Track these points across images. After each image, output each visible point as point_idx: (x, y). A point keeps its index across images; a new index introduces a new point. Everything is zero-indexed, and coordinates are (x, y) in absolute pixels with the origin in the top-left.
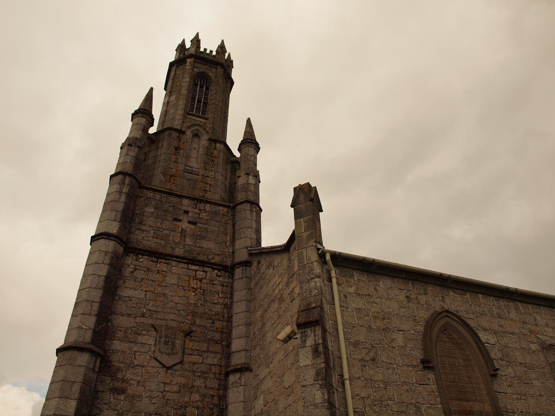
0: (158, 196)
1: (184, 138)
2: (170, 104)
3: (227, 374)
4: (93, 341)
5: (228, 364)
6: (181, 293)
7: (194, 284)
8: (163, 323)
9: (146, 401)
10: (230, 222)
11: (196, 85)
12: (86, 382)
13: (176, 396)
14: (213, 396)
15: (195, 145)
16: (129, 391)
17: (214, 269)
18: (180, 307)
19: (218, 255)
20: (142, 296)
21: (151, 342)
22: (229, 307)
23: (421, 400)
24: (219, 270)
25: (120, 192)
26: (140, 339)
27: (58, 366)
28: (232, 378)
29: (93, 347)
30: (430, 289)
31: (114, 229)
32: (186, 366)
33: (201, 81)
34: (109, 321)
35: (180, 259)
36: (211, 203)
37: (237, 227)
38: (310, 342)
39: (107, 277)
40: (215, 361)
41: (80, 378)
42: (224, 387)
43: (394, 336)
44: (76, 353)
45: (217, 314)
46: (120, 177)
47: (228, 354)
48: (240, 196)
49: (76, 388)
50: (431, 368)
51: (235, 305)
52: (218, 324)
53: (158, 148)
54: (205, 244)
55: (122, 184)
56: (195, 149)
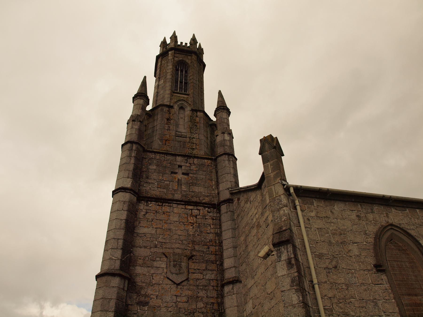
0: (158, 156)
1: (172, 111)
2: (160, 87)
3: (223, 286)
4: (121, 268)
5: (223, 279)
7: (191, 219)
8: (171, 251)
9: (164, 310)
10: (214, 171)
11: (177, 70)
12: (119, 299)
13: (186, 305)
14: (213, 303)
15: (182, 116)
16: (151, 303)
17: (205, 207)
18: (182, 238)
19: (207, 196)
20: (154, 232)
21: (164, 265)
22: (219, 235)
24: (209, 208)
25: (130, 156)
26: (155, 264)
27: (98, 288)
28: (227, 289)
29: (121, 273)
31: (128, 184)
32: (191, 282)
33: (181, 67)
34: (131, 252)
35: (178, 202)
36: (198, 158)
38: (284, 257)
40: (213, 277)
41: (114, 296)
42: (221, 296)
43: (350, 247)
44: (110, 278)
45: (211, 241)
46: (129, 145)
47: (221, 270)
48: (220, 151)
49: (113, 304)
50: (383, 271)
51: (224, 233)
52: (212, 249)
53: (154, 120)
54: (197, 189)
55: (131, 150)
56: (182, 118)
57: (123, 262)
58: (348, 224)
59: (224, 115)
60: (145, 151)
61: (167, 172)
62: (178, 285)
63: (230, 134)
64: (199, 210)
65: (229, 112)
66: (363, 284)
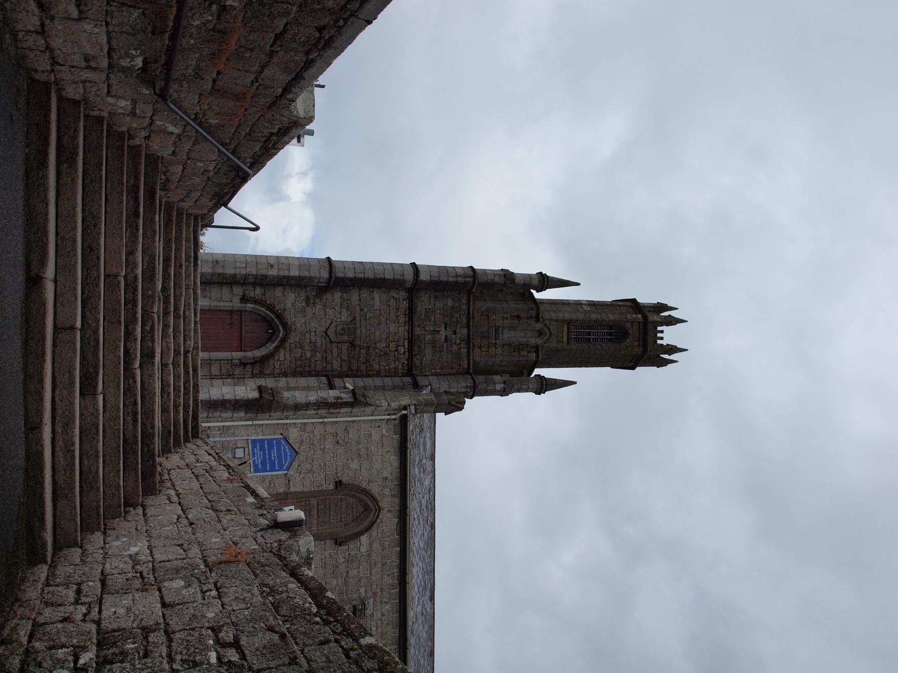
0: (464, 307)
1: (532, 322)
2: (579, 307)
3: (326, 376)
4: (337, 278)
5: (334, 376)
6: (384, 336)
7: (393, 345)
8: (358, 325)
9: (303, 320)
11: (611, 328)
12: (311, 278)
14: (310, 366)
15: (529, 334)
16: (308, 308)
17: (408, 360)
18: (372, 336)
19: (421, 363)
20: (376, 307)
21: (343, 319)
22: (378, 374)
23: (315, 475)
24: (408, 365)
25: (457, 276)
26: (344, 311)
27: (319, 260)
28: (324, 379)
29: (333, 279)
30: (397, 500)
31: (424, 277)
32: (329, 346)
33: (617, 332)
34: (354, 287)
35: (411, 332)
36: (469, 352)
37: (449, 377)
38: (343, 395)
39: (384, 279)
41: (312, 275)
42: (318, 374)
43: (356, 461)
44: (328, 269)
45: (371, 366)
46: (471, 273)
47: (342, 375)
48: (480, 378)
49: (306, 274)
52: (363, 367)
54: (428, 351)
57: (343, 279)
58: (378, 466)
59: (535, 386)
60: (469, 292)
61: (446, 319)
62: (326, 333)
63: (504, 393)
64: (404, 354)
65: (539, 392)
66: (325, 465)
